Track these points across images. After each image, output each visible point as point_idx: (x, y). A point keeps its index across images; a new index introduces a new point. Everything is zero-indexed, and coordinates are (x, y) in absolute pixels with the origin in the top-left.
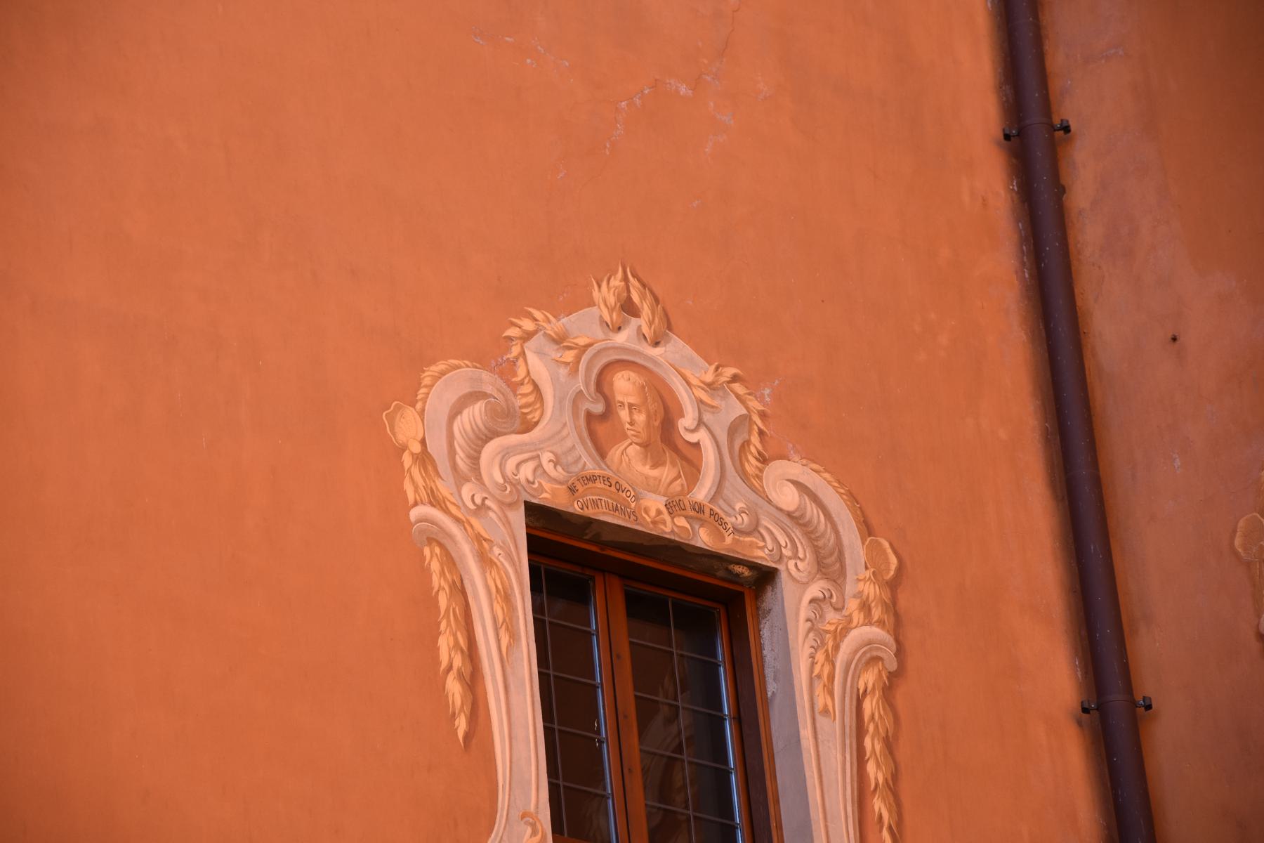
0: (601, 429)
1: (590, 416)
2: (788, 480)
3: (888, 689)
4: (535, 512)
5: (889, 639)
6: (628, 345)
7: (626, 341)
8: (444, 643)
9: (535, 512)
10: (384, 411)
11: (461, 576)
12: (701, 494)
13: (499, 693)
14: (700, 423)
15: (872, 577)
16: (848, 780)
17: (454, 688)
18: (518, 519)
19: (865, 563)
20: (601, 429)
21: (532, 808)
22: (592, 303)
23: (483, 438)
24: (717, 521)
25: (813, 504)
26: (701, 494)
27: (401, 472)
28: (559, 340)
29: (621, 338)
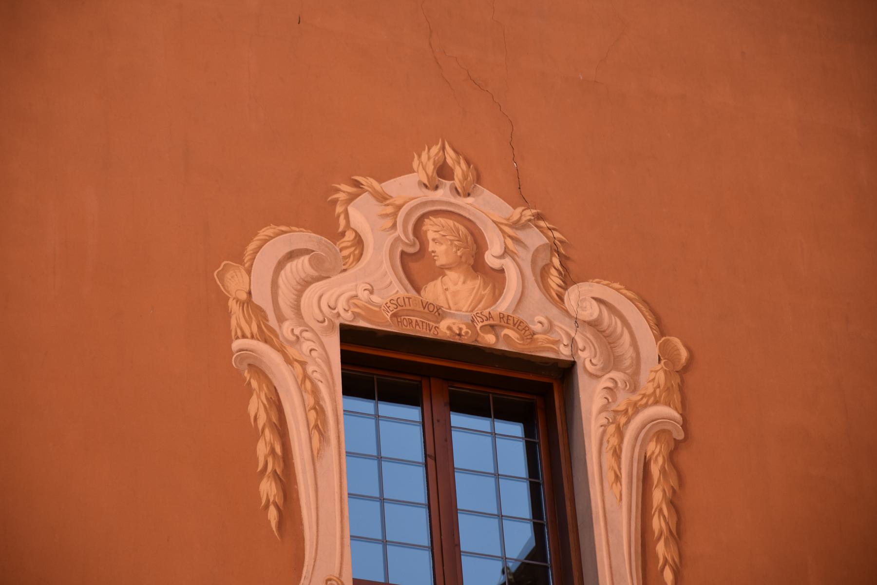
0: (414, 266)
1: (403, 253)
2: (593, 298)
3: (672, 458)
4: (348, 334)
5: (676, 415)
6: (445, 199)
7: (526, 559)
8: (262, 449)
9: (348, 334)
10: (214, 271)
11: (275, 388)
12: (504, 305)
13: (309, 497)
14: (506, 252)
15: (664, 367)
16: (634, 564)
17: (268, 488)
18: (334, 346)
19: (659, 356)
20: (414, 266)
21: (336, 573)
22: (411, 171)
23: (306, 283)
24: (519, 325)
25: (616, 317)
26: (504, 305)
27: (227, 314)
28: (382, 198)
29: (439, 194)
